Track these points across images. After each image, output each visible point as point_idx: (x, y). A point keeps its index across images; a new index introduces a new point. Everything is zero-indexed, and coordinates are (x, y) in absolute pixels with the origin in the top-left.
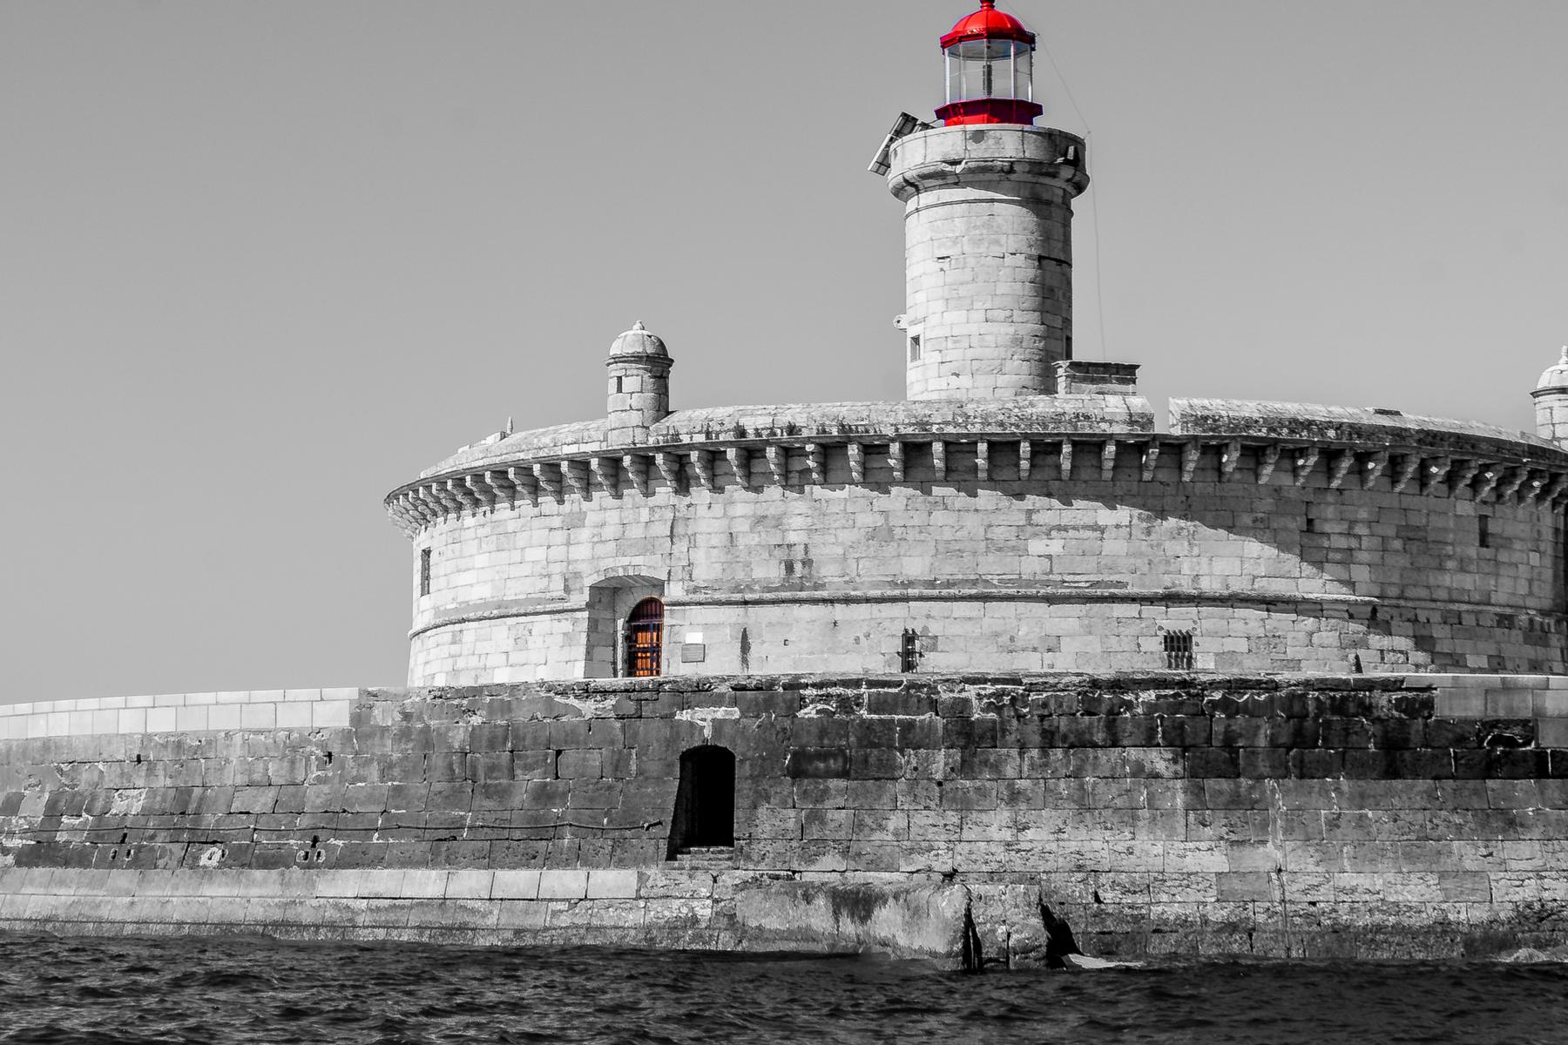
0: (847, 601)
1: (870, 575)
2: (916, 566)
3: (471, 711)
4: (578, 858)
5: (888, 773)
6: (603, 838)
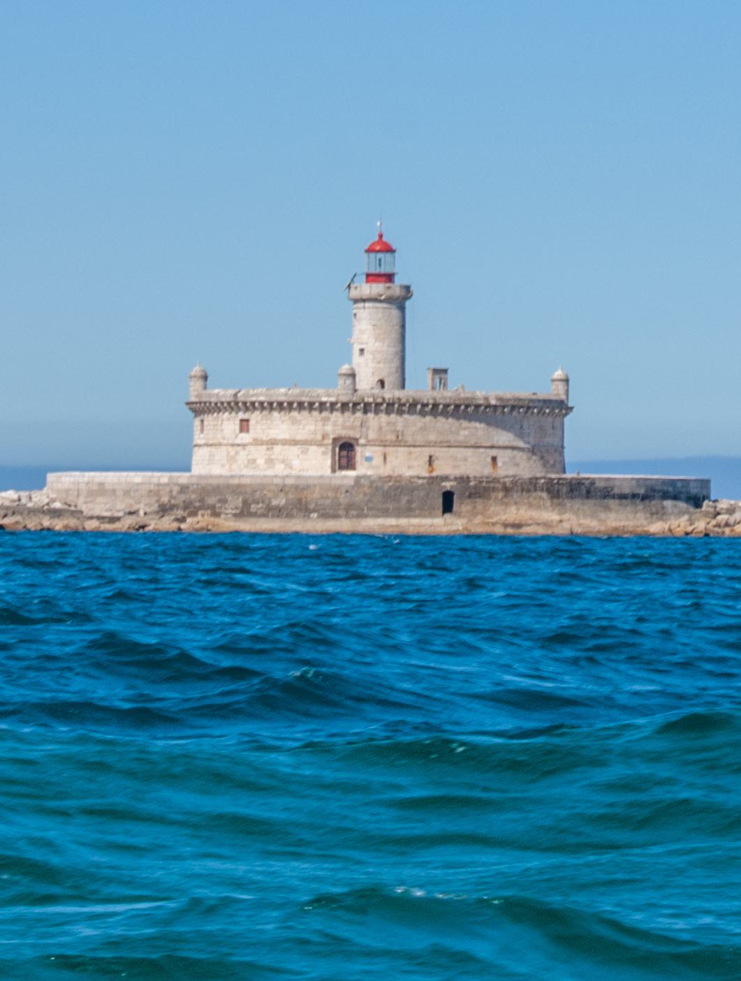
0: (414, 446)
1: (420, 439)
2: (432, 437)
3: (390, 481)
4: (419, 516)
5: (489, 498)
6: (425, 511)
